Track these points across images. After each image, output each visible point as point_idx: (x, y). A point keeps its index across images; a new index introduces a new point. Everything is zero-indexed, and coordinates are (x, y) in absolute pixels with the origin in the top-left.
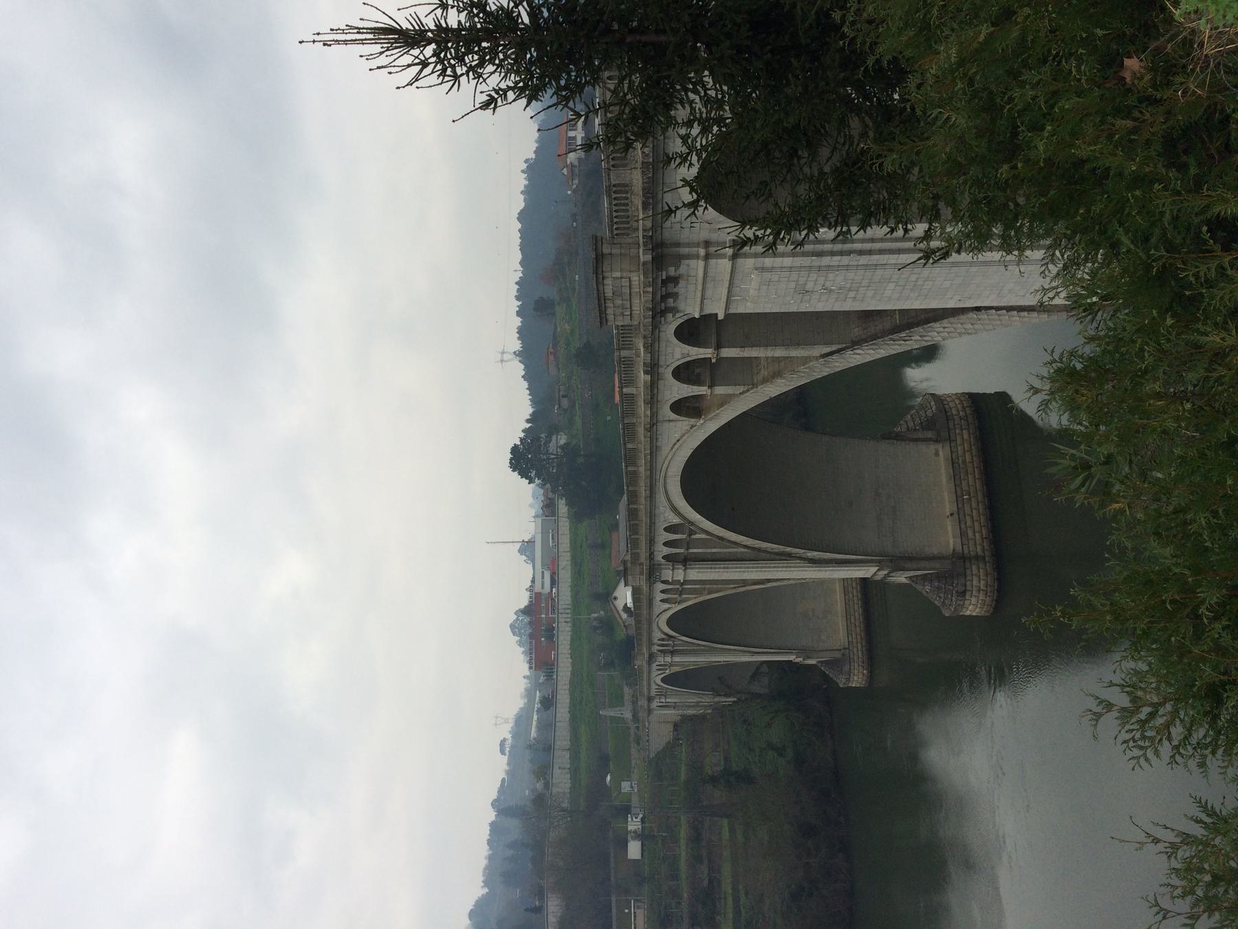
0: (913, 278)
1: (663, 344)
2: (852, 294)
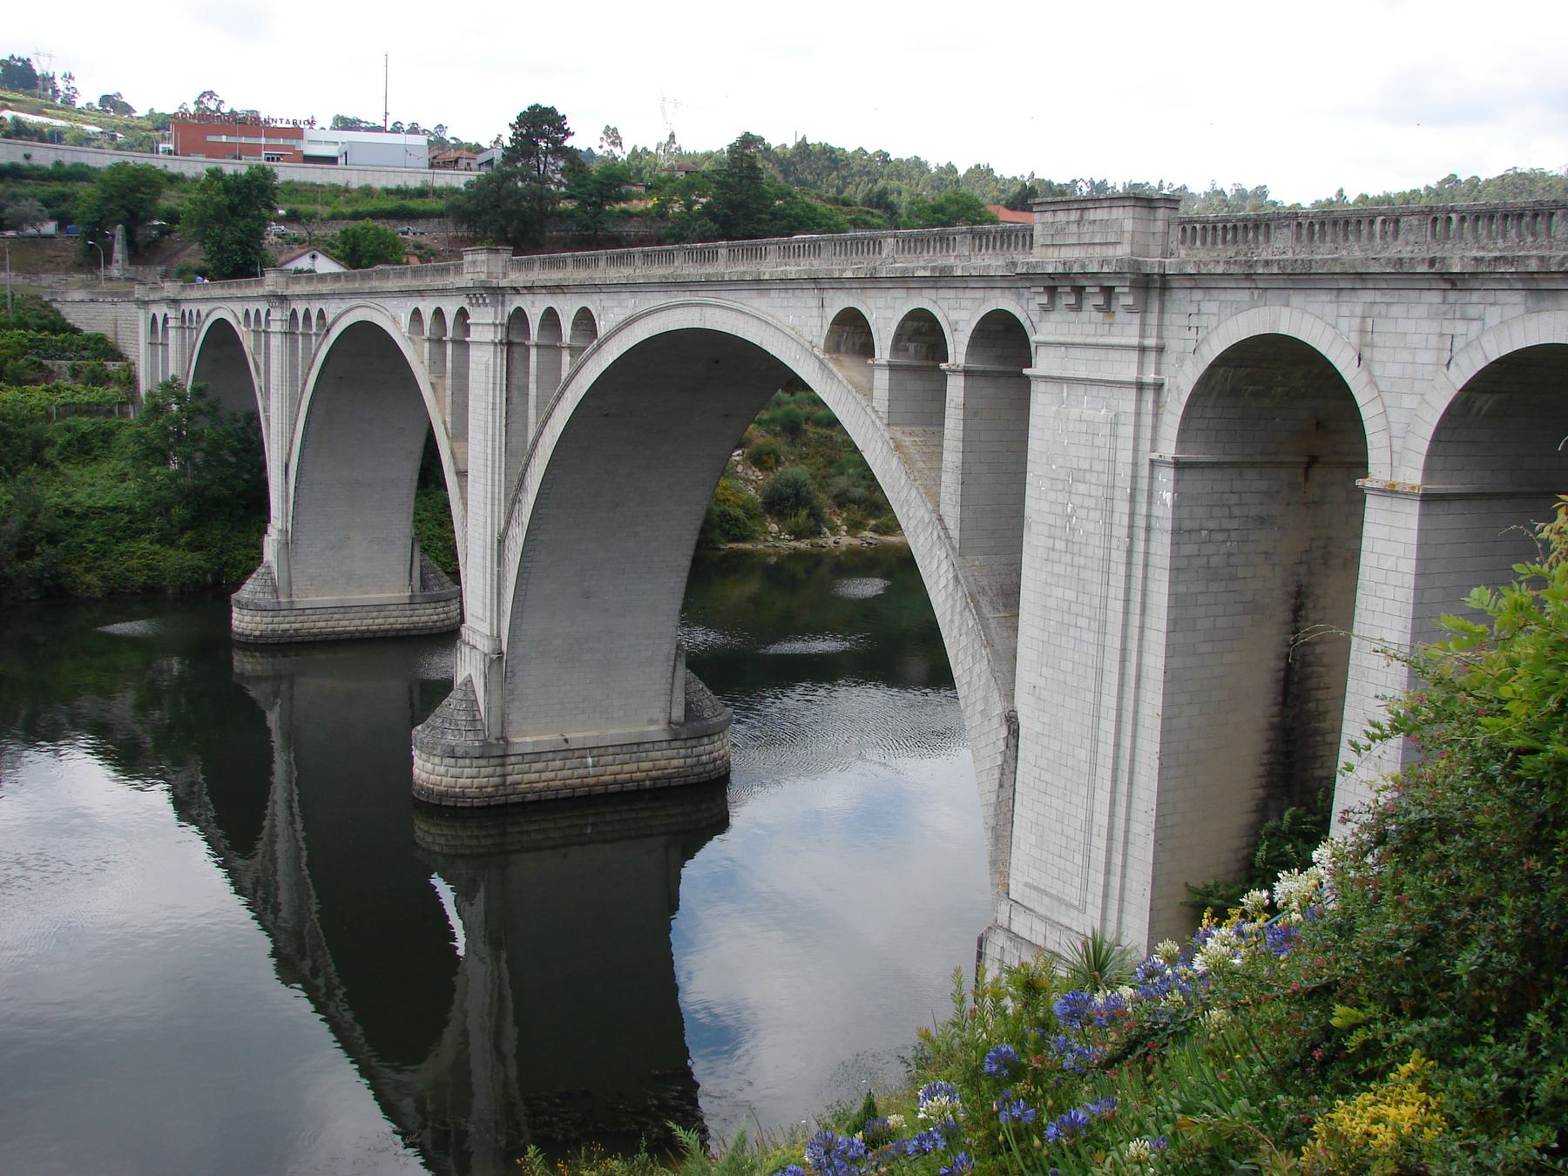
0: (1083, 622)
1: (979, 294)
2: (1060, 545)
